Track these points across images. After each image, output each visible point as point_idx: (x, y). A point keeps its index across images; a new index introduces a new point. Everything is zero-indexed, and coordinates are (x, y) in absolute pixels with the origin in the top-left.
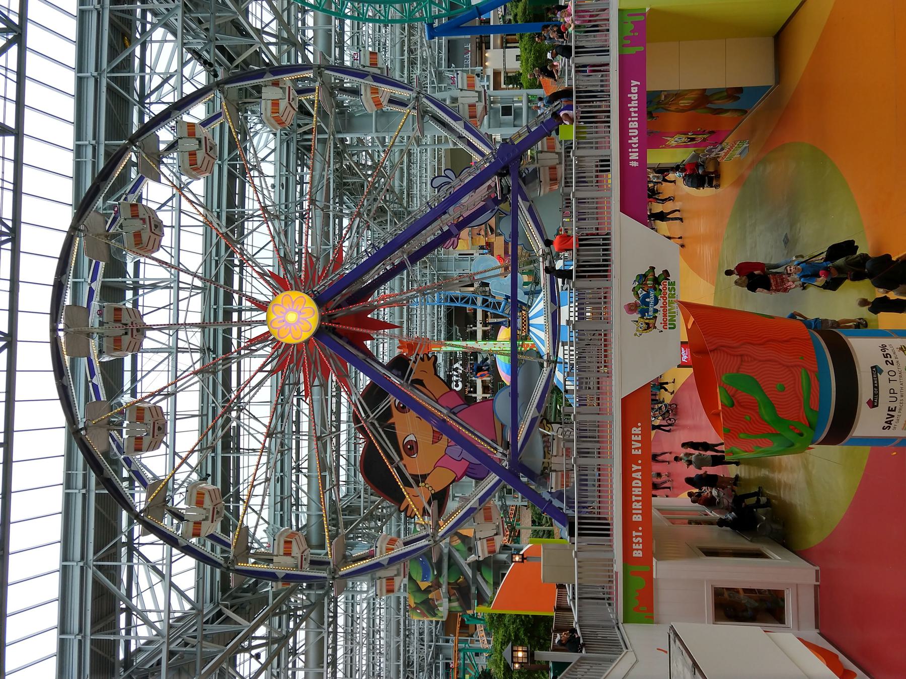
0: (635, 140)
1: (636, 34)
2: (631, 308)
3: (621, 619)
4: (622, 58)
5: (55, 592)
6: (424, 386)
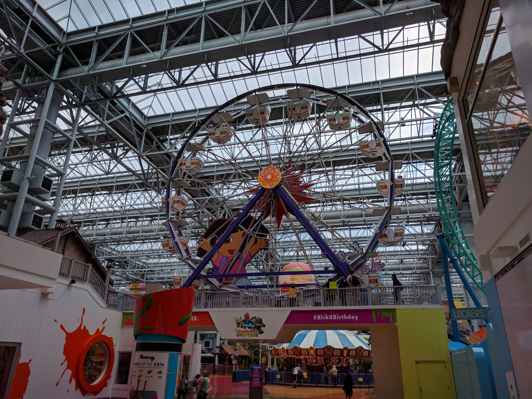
0: (327, 318)
1: (383, 318)
2: (247, 316)
3: (124, 312)
4: (370, 311)
5: (187, 109)
6: (254, 244)
